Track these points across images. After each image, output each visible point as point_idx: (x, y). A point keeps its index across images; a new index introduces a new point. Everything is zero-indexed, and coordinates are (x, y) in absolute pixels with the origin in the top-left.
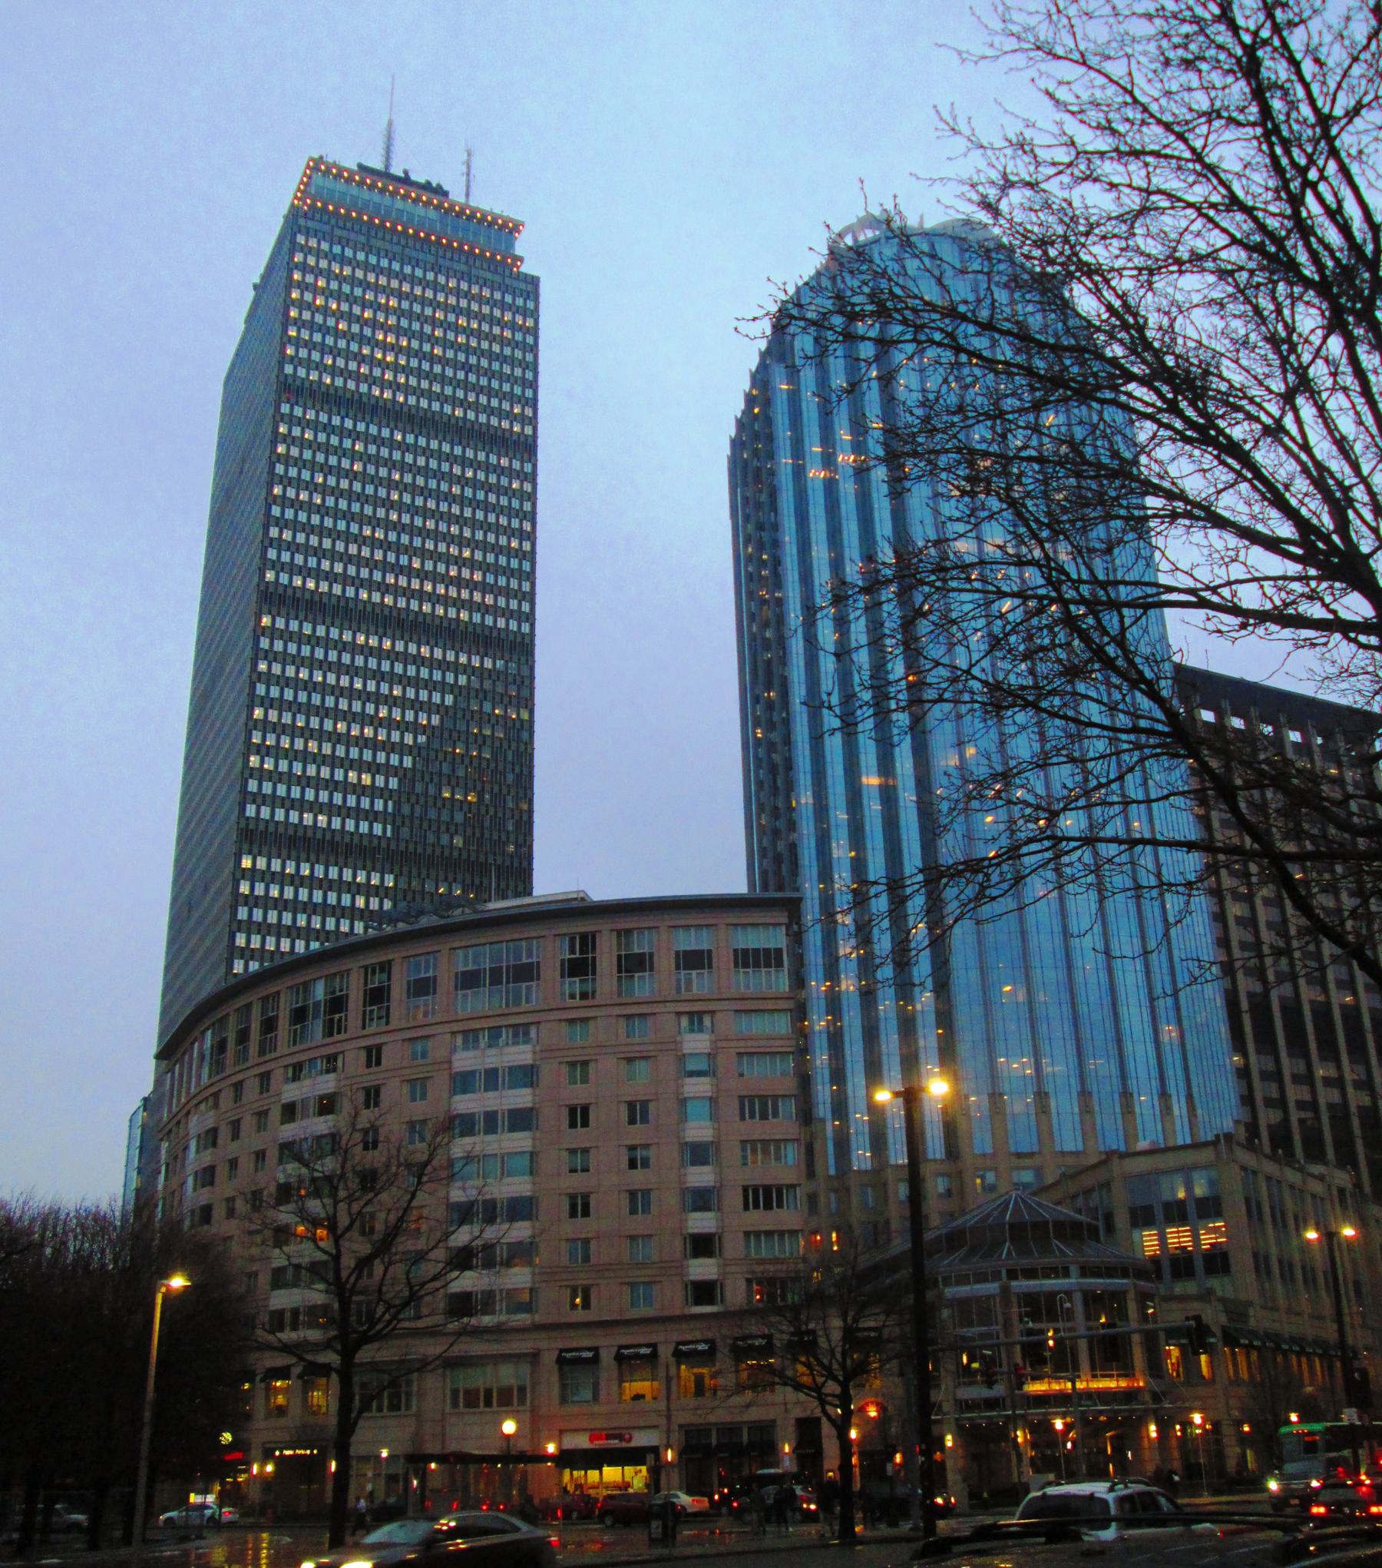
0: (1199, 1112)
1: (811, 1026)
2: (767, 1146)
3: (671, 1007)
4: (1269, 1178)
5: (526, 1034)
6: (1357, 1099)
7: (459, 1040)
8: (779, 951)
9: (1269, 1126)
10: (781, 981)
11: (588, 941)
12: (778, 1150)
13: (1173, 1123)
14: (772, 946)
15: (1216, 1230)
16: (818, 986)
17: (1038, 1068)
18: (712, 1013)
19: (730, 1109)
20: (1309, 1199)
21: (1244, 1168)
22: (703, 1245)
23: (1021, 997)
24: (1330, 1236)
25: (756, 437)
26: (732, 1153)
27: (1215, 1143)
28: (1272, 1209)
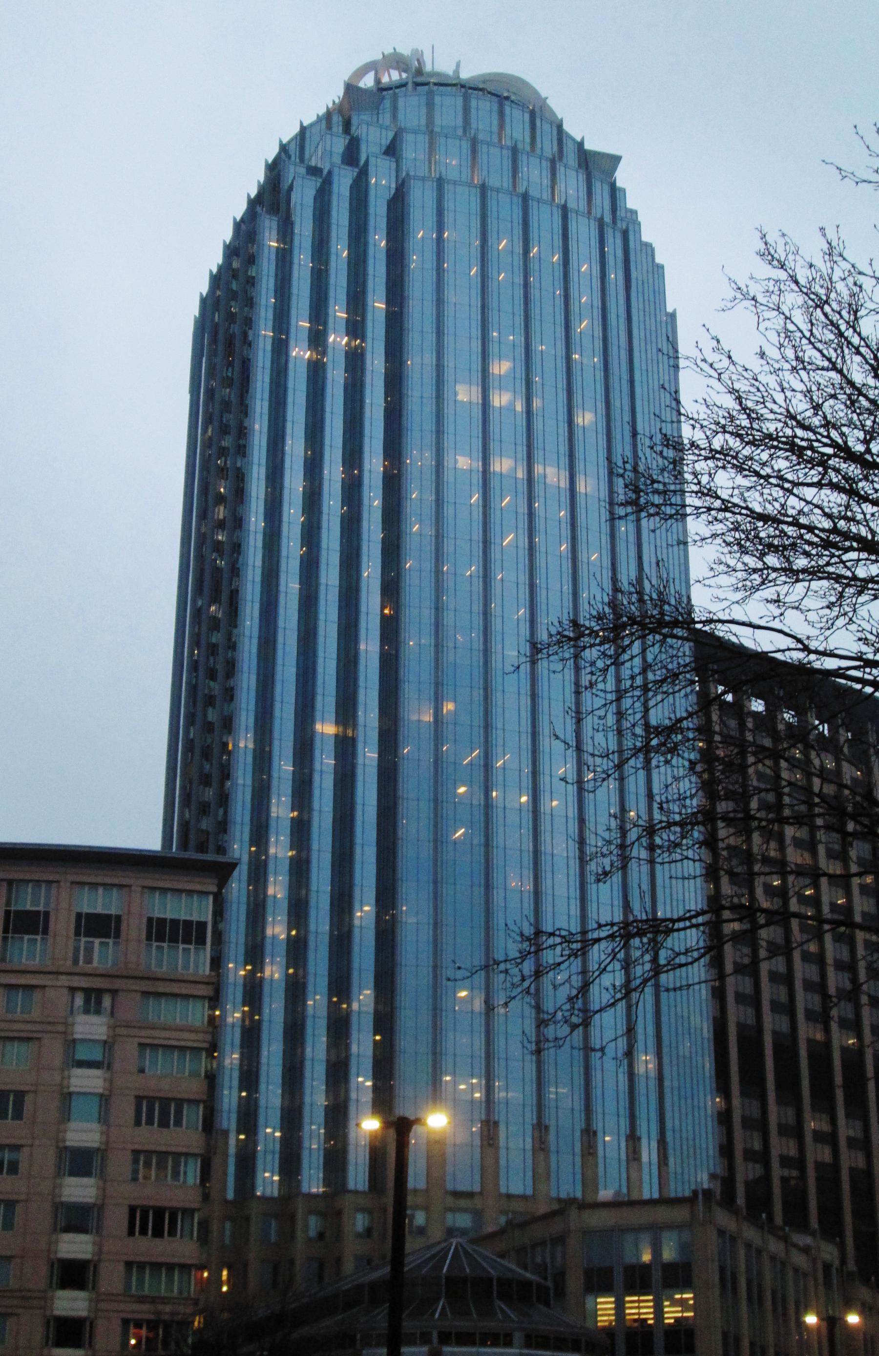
0: (671, 1160)
1: (223, 1016)
2: (166, 1160)
3: (64, 981)
4: (748, 1246)
6: (850, 1160)
7: (79, 1000)
8: (202, 926)
9: (747, 1183)
10: (199, 962)
12: (176, 1166)
13: (640, 1170)
14: (195, 918)
15: (682, 1303)
16: (237, 971)
17: (489, 1090)
18: (114, 992)
19: (124, 1109)
20: (791, 1274)
21: (721, 1232)
22: (73, 1274)
23: (478, 1005)
24: (832, 1322)
25: (233, 296)
26: (120, 1164)
27: (692, 1200)
28: (749, 1282)
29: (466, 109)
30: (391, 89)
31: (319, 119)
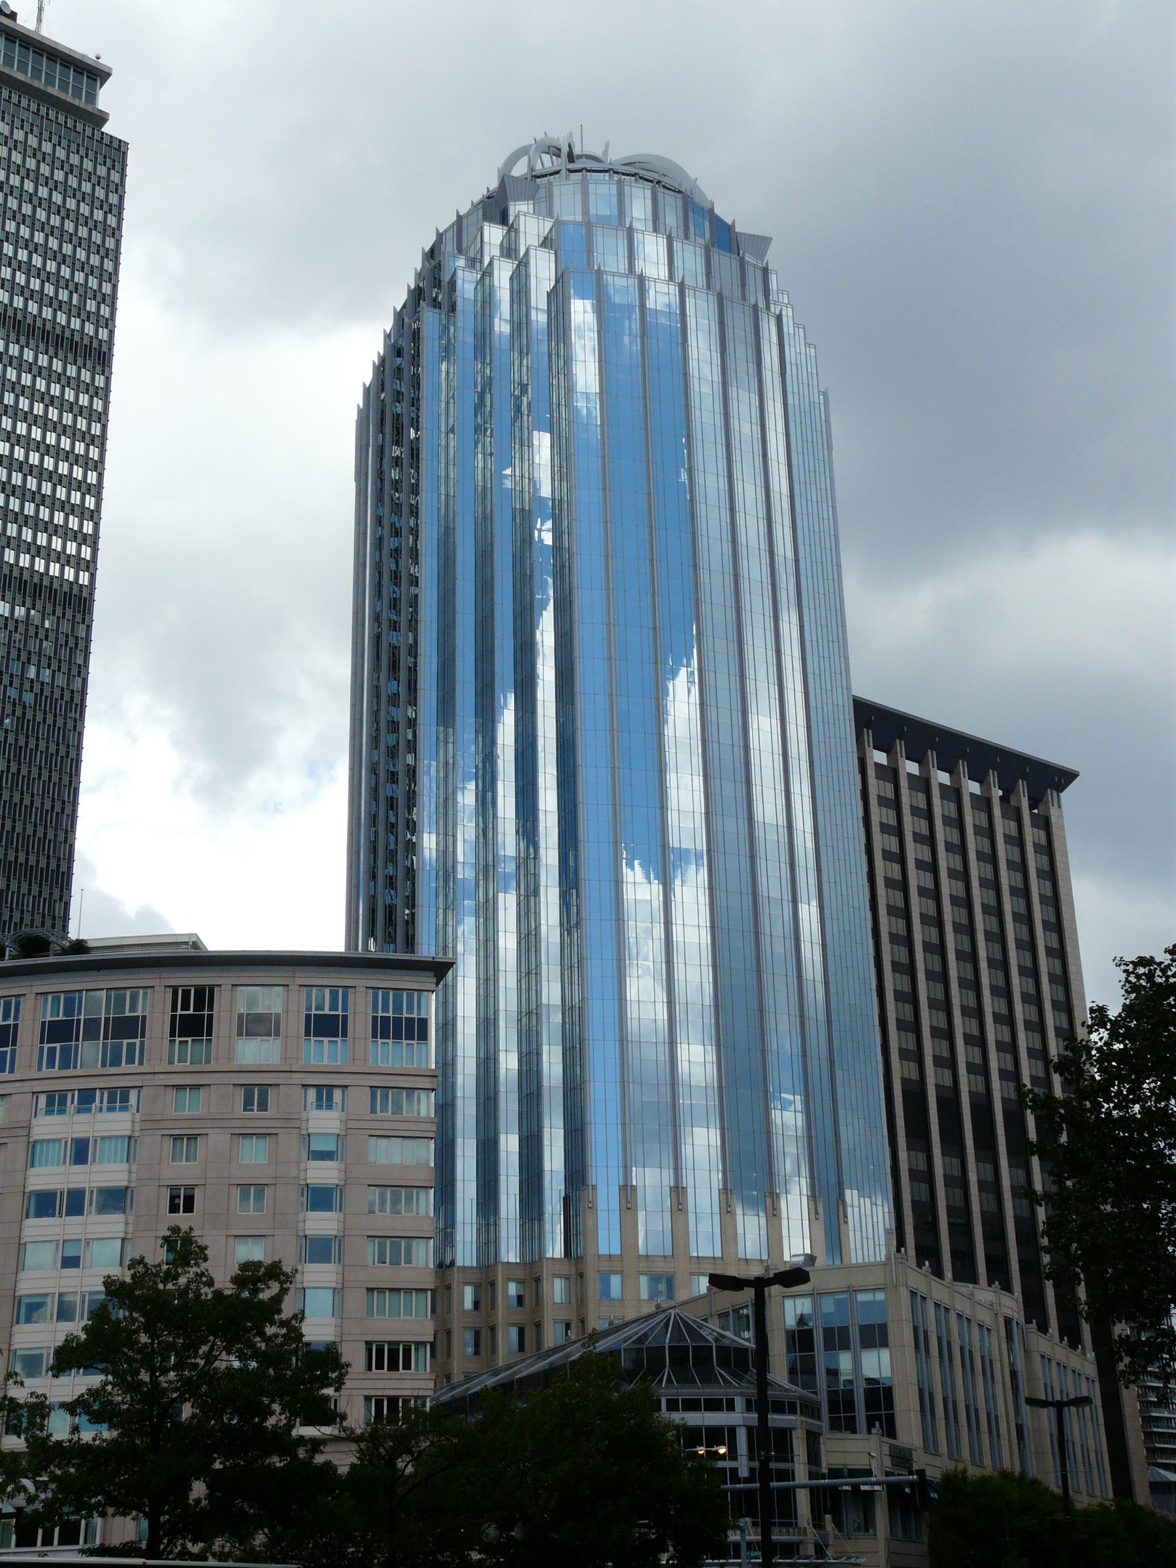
5: (125, 1098)
11: (205, 996)
18: (344, 1087)
20: (975, 1328)
29: (621, 195)
30: (545, 176)
31: (475, 206)
